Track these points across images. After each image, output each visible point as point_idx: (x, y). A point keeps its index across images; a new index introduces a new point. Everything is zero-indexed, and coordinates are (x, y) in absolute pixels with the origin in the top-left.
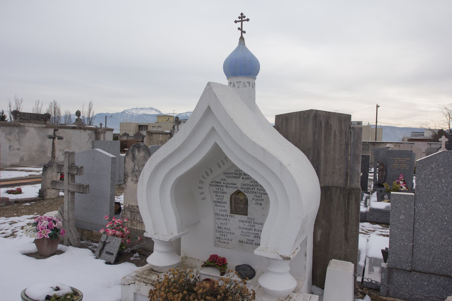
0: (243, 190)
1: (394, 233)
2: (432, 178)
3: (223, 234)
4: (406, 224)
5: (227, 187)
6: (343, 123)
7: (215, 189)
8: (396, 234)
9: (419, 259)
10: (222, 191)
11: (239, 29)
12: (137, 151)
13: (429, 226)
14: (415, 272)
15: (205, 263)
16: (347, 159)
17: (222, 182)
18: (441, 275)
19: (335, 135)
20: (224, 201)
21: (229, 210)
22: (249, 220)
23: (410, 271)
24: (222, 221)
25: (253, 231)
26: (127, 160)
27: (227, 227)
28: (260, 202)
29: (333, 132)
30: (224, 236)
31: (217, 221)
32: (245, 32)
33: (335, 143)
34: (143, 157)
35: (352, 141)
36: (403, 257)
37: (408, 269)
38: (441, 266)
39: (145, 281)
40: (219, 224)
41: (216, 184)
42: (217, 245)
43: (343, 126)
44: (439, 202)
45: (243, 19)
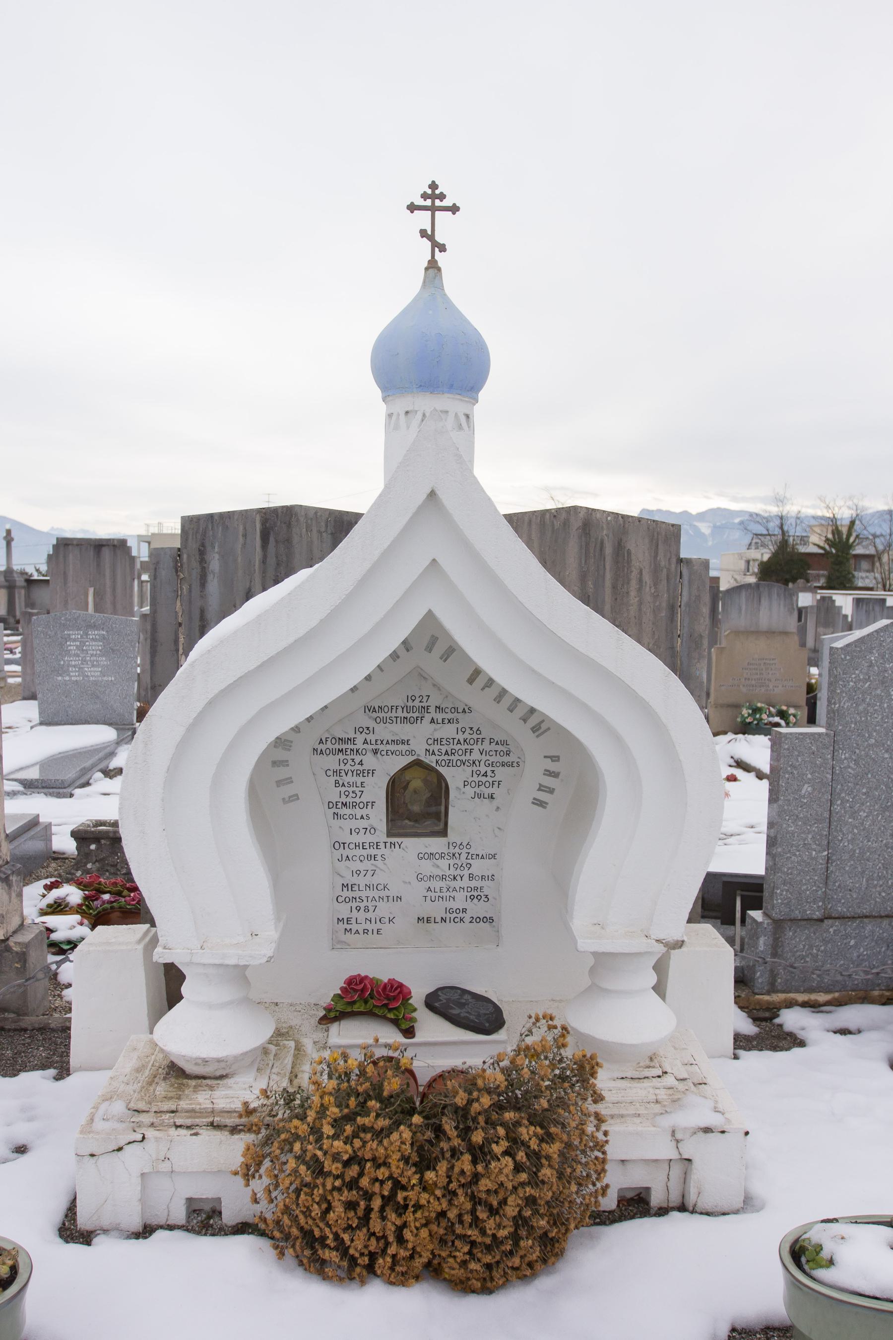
0: (434, 758)
1: (788, 832)
2: (869, 687)
3: (362, 905)
4: (815, 806)
5: (375, 752)
6: (661, 546)
7: (332, 762)
8: (793, 833)
9: (839, 886)
10: (359, 767)
13: (863, 804)
14: (830, 921)
15: (328, 1009)
16: (672, 648)
17: (360, 739)
18: (881, 917)
19: (640, 581)
20: (364, 799)
22: (452, 850)
23: (821, 920)
24: (356, 865)
25: (466, 883)
27: (375, 880)
28: (487, 791)
29: (634, 575)
30: (367, 909)
32: (443, 248)
33: (640, 603)
35: (685, 598)
36: (807, 890)
37: (818, 915)
38: (884, 894)
39: (179, 1122)
41: (337, 746)
42: (340, 942)
44: (883, 745)
45: (438, 203)
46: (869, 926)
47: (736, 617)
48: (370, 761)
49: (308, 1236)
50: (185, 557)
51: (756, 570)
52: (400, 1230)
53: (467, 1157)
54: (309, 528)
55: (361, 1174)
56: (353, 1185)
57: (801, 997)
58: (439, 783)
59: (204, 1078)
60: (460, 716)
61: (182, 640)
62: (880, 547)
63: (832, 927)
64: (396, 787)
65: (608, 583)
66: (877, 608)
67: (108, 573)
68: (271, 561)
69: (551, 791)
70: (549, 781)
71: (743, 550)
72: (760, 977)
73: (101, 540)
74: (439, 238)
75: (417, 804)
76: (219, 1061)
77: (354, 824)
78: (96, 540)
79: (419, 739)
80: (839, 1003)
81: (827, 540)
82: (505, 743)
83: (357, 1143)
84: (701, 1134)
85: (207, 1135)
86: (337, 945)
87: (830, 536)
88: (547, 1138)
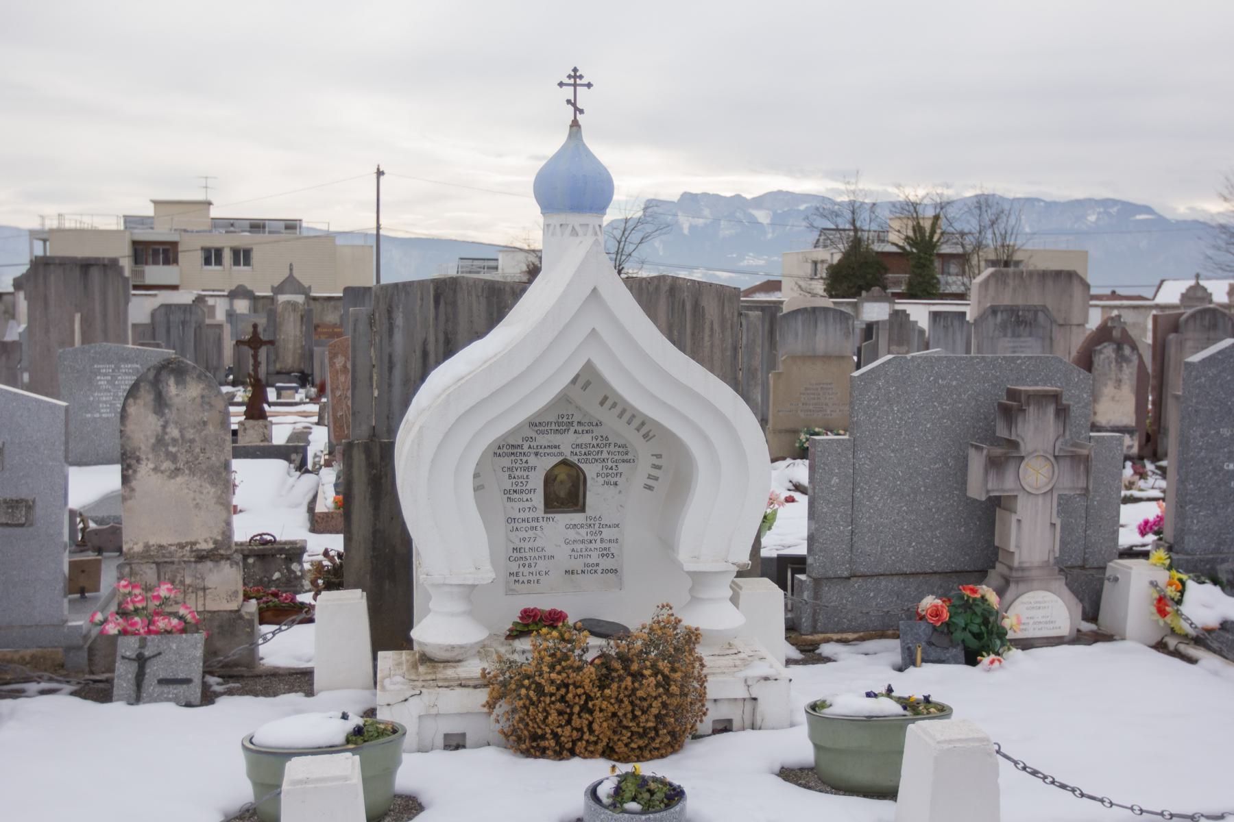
5: (536, 454)
7: (506, 461)
11: (569, 102)
12: (172, 381)
15: (511, 630)
17: (526, 445)
19: (712, 329)
21: (541, 506)
23: (848, 578)
24: (523, 534)
25: (598, 545)
26: (132, 410)
27: (536, 544)
28: (613, 480)
30: (530, 566)
31: (513, 535)
32: (581, 111)
33: (712, 346)
34: (199, 400)
35: (744, 342)
37: (846, 574)
40: (517, 541)
43: (726, 309)
45: (578, 81)
46: (884, 582)
47: (793, 342)
48: (533, 460)
49: (535, 737)
50: (377, 315)
51: (824, 275)
52: (591, 723)
53: (629, 679)
54: (469, 293)
55: (567, 692)
56: (563, 699)
57: (835, 636)
58: (578, 476)
59: (448, 662)
60: (594, 428)
61: (375, 377)
62: (969, 248)
63: (856, 584)
64: (549, 480)
65: (689, 331)
66: (956, 323)
67: (97, 296)
68: (442, 318)
69: (656, 479)
70: (655, 472)
71: (809, 248)
72: (806, 623)
73: (88, 259)
74: (579, 105)
75: (565, 492)
76: (461, 647)
77: (521, 505)
78: (83, 259)
79: (566, 445)
80: (862, 639)
81: (907, 238)
82: (624, 446)
83: (564, 675)
84: (763, 682)
85: (459, 690)
86: (510, 592)
87: (911, 234)
88: (674, 670)
